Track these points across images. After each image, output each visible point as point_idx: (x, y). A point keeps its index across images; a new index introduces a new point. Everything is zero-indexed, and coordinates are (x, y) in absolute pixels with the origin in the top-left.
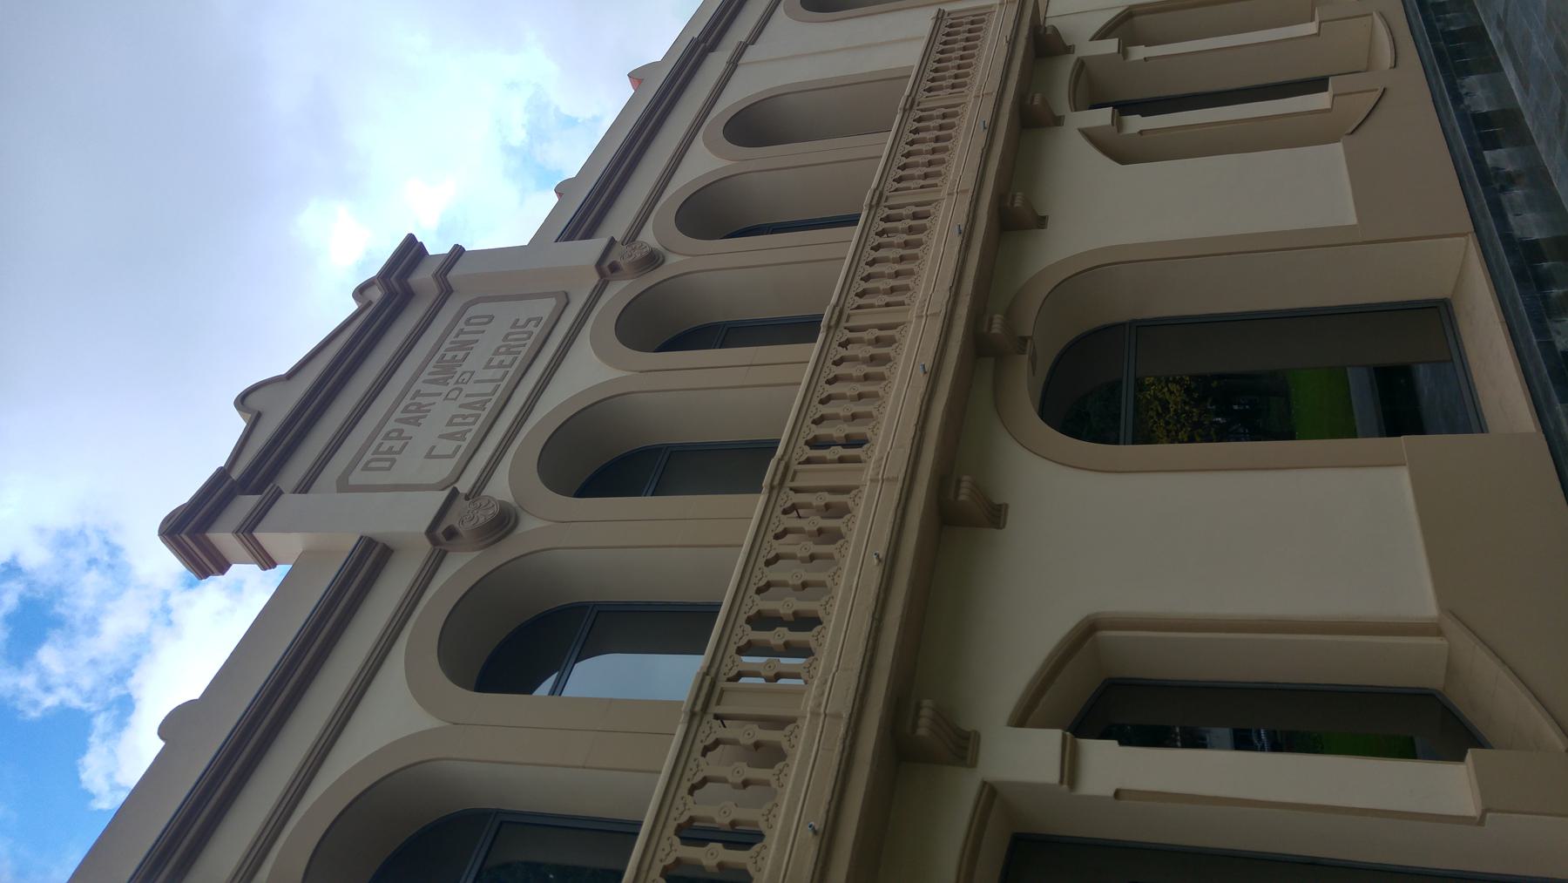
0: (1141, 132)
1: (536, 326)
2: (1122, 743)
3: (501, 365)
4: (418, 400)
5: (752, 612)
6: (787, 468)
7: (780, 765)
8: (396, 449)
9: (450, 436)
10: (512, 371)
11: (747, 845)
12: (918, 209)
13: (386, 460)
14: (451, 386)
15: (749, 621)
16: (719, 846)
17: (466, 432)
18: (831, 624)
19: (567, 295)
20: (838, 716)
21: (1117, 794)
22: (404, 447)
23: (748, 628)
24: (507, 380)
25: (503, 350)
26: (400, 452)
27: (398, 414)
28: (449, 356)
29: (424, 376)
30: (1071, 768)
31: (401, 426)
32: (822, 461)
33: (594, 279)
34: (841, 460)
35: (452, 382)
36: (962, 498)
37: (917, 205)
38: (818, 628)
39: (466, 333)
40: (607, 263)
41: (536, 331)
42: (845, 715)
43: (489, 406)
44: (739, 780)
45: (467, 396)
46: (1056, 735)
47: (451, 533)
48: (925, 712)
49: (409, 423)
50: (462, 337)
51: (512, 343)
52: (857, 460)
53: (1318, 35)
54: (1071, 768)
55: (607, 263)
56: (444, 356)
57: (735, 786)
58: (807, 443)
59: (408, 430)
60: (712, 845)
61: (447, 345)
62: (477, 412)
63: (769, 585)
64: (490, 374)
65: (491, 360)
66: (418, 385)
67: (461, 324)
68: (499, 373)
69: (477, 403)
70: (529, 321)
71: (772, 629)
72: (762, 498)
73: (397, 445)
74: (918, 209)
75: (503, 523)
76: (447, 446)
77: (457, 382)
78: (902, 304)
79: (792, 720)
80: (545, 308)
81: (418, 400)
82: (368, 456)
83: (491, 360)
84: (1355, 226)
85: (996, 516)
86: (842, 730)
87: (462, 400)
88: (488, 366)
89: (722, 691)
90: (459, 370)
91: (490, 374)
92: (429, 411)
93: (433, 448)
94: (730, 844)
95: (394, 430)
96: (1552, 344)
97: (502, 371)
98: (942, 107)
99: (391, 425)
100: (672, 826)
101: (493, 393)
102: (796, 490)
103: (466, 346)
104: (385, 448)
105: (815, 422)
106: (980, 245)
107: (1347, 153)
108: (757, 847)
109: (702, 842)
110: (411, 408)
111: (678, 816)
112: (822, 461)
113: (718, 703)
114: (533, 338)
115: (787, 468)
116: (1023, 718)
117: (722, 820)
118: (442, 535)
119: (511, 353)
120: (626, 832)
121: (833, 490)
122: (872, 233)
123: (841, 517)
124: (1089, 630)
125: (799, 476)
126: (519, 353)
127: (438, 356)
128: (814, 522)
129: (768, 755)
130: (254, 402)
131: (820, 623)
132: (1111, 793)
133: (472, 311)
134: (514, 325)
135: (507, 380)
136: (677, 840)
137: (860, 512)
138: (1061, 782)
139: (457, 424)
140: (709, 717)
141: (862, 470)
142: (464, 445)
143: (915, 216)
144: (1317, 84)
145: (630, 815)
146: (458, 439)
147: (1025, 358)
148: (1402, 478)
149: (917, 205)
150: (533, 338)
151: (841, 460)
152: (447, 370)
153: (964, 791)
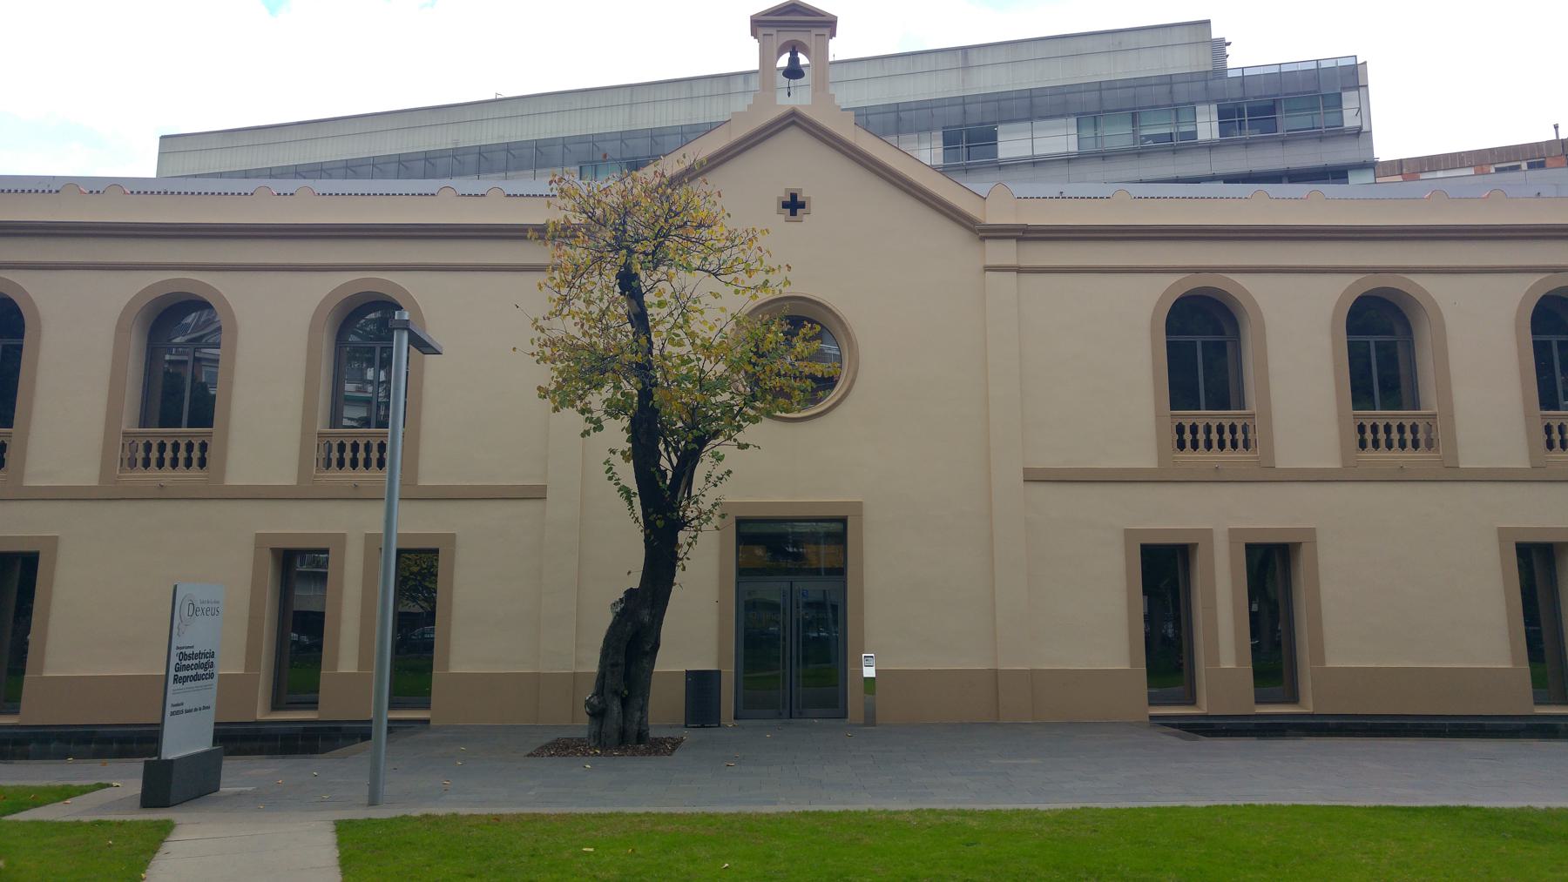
71: (1372, 432)
131: (1390, 449)
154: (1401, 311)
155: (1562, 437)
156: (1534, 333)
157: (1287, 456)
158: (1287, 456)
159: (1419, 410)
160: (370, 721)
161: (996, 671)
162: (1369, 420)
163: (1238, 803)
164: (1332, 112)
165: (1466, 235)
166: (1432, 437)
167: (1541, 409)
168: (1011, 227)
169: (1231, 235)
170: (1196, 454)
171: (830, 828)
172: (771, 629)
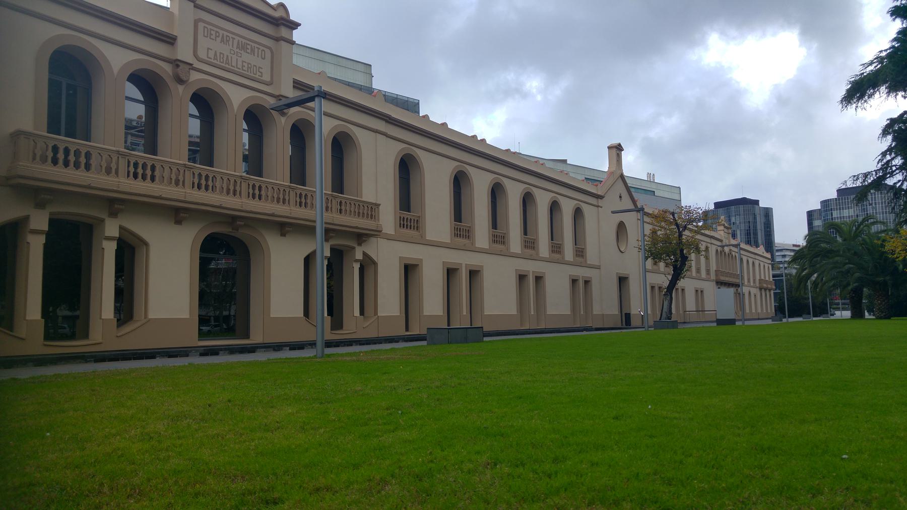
0: (353, 267)
1: (259, 76)
2: (116, 250)
3: (243, 66)
4: (231, 39)
5: (155, 165)
6: (296, 189)
7: (106, 174)
8: (248, 51)
9: (216, 54)
10: (241, 71)
11: (198, 188)
12: (330, 208)
13: (207, 34)
14: (236, 50)
15: (254, 184)
16: (85, 162)
17: (217, 60)
18: (152, 185)
19: (272, 84)
20: (119, 188)
21: (28, 243)
22: (249, 53)
23: (151, 164)
24: (238, 70)
25: (250, 66)
26: (210, 38)
27: (226, 33)
28: (248, 47)
29: (241, 39)
30: (357, 261)
31: (221, 36)
32: (296, 197)
33: (277, 93)
34: (249, 193)
35: (238, 50)
36: (181, 214)
37: (331, 208)
38: (151, 182)
39: (258, 51)
40: (179, 63)
41: (257, 76)
42: (119, 189)
43: (227, 66)
44: (164, 176)
45: (231, 57)
46: (118, 236)
47: (178, 66)
48: (186, 215)
49: (222, 39)
50: (256, 50)
51: (252, 69)
52: (296, 205)
53: (353, 316)
54: (357, 261)
55: (179, 63)
56: (249, 45)
57: (100, 163)
58: (254, 184)
59: (219, 39)
60: (85, 160)
61: (253, 45)
62: (225, 62)
63: (346, 203)
64: (240, 63)
65: (246, 62)
66: (237, 38)
67: (262, 48)
68: (240, 66)
69: (228, 62)
70: (261, 73)
71: (205, 180)
72: (330, 193)
73: (213, 37)
74: (330, 208)
75: (180, 81)
76: (211, 54)
77: (237, 52)
78: (296, 205)
79: (118, 176)
80: (267, 77)
81: (231, 39)
82: (209, 27)
83: (246, 62)
84: (270, 315)
85: (283, 235)
86: (115, 189)
87: (230, 55)
88: (243, 62)
89: (29, 139)
90: (242, 52)
91: (240, 63)
92: (226, 44)
93: (211, 50)
94: (305, 203)
95: (219, 35)
96: (222, 350)
97: (241, 67)
98: (241, 189)
99: (221, 32)
100: (145, 161)
101: (232, 66)
102: (289, 192)
103: (253, 51)
104: (212, 32)
105: (345, 202)
106: (80, 191)
107: (36, 320)
108: (85, 170)
109: (86, 157)
110: (228, 38)
111: (92, 151)
112: (296, 197)
113: (188, 170)
114: (254, 76)
115: (296, 189)
116: (121, 228)
117: (91, 162)
118: (176, 63)
119: (248, 69)
120: (88, 139)
121: (184, 182)
122: (359, 203)
123: (142, 178)
124: (146, 244)
125: (245, 183)
126: (248, 72)
127: (249, 42)
128: (281, 196)
129: (108, 171)
130: (677, 191)
131: (66, 167)
132: (28, 241)
133: (267, 51)
134: (259, 68)
135: (238, 70)
136: (86, 151)
137: (228, 198)
138: (31, 230)
139: (220, 56)
140: (118, 155)
141: (246, 198)
142: (212, 61)
143: (372, 215)
144: (362, 312)
145: (215, 164)
146: (214, 57)
147: (231, 230)
148: (186, 315)
149: (331, 208)
150: (254, 76)
151: (249, 193)
152: (243, 47)
153: (355, 245)
154: (341, 147)
155: (199, 181)
156: (50, 73)
157: (430, 236)
158: (430, 236)
159: (156, 156)
160: (315, 341)
161: (603, 314)
162: (142, 160)
163: (176, 365)
164: (900, 319)
165: (408, 128)
166: (48, 155)
167: (400, 210)
168: (363, 106)
169: (338, 100)
170: (65, 170)
171: (131, 385)
172: (681, 313)
